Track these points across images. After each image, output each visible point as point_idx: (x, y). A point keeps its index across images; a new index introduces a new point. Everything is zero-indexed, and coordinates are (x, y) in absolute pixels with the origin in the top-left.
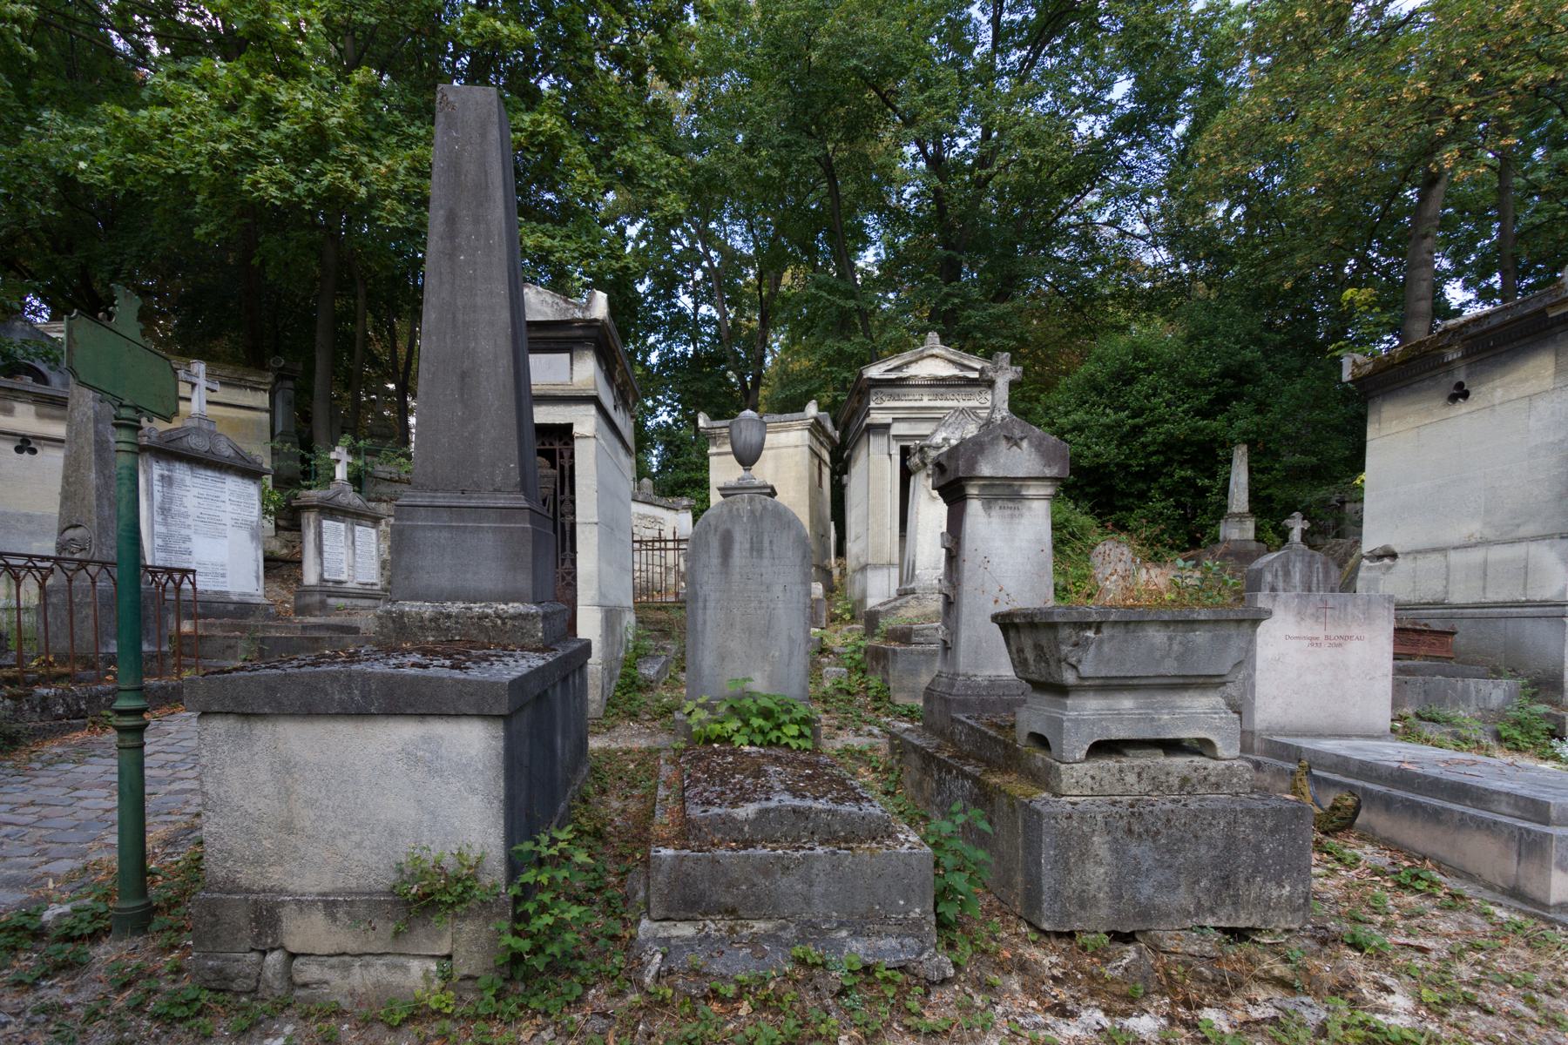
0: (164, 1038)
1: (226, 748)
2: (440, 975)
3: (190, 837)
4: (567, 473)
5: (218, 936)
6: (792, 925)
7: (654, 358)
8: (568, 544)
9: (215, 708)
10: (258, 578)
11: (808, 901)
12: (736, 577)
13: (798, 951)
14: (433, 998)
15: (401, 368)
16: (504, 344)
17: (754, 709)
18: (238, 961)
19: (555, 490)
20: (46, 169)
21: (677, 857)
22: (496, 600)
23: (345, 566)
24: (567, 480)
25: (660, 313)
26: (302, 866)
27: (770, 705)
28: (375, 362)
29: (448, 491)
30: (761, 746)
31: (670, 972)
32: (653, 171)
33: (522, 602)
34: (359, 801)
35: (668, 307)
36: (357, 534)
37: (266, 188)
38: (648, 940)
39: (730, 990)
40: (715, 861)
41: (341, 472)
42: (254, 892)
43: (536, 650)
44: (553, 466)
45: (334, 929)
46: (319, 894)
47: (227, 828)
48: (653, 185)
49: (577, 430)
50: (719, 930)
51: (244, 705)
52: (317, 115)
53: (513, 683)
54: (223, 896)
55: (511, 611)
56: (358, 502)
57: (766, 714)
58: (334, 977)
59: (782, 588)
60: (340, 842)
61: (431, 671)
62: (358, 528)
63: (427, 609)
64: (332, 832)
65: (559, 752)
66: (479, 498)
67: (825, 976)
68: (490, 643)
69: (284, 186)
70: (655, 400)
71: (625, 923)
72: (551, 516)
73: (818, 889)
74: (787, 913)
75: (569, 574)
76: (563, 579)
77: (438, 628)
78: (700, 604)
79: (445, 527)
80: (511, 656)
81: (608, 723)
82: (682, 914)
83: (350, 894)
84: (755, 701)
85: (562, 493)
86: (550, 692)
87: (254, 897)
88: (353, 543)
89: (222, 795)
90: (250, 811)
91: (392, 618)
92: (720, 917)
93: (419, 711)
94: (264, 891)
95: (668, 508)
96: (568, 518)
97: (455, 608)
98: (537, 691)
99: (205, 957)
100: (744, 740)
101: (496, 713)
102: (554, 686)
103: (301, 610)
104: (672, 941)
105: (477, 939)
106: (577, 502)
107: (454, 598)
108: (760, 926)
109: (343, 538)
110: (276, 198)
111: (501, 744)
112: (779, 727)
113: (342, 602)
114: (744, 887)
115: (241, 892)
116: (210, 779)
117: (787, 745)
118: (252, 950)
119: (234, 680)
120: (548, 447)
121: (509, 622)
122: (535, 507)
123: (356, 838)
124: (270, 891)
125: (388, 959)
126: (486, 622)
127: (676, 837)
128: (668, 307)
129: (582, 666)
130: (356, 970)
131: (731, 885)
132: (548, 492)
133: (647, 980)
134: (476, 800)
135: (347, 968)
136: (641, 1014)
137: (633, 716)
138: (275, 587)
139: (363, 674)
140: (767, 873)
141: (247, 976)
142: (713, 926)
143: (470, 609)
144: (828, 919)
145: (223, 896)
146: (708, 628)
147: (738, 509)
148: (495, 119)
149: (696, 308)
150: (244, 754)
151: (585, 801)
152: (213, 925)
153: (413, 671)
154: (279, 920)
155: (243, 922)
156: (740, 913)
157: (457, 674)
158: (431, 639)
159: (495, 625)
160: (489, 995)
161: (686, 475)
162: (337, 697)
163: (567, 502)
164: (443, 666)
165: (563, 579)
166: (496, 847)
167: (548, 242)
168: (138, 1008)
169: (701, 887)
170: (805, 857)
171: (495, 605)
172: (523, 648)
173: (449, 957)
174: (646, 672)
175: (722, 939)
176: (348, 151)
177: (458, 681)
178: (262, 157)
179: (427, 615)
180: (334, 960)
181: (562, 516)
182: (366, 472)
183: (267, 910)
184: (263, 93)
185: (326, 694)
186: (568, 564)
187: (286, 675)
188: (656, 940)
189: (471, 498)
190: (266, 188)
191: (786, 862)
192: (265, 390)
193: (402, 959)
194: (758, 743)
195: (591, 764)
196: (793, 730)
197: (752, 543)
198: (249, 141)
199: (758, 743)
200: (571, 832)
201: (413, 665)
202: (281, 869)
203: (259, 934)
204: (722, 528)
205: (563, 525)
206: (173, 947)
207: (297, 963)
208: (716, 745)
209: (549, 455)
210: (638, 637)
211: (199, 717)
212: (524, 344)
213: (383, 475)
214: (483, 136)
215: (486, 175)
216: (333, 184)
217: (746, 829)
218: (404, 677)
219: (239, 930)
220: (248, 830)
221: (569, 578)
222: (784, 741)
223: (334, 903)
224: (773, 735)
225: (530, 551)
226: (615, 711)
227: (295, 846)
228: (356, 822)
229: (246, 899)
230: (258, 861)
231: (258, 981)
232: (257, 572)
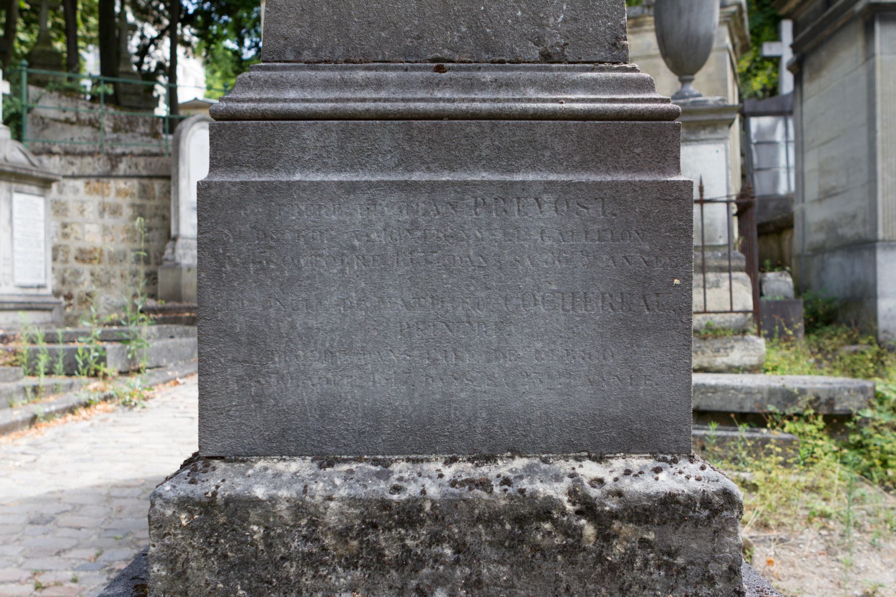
36: (16, 206)
62: (17, 197)
171: (564, 466)
179: (333, 514)
189: (471, 85)
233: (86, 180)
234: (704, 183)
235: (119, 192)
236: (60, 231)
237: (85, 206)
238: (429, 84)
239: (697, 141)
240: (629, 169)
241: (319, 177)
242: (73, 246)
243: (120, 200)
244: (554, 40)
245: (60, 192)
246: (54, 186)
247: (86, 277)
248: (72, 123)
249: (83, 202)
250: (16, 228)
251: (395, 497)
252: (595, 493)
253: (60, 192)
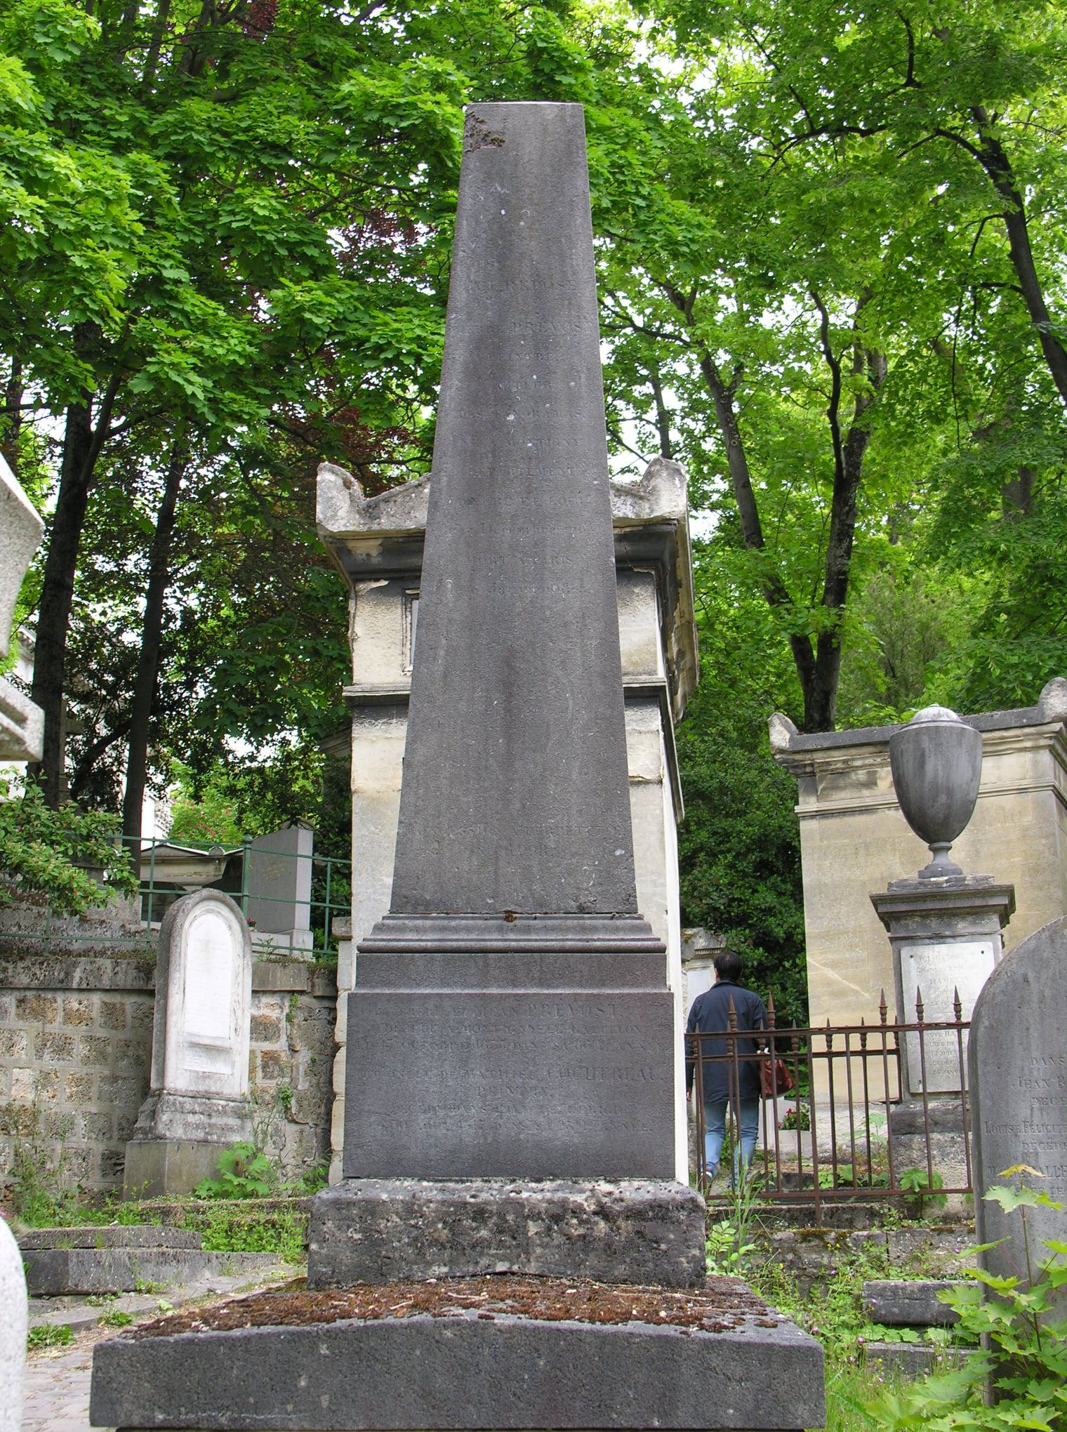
189: (528, 930)
234: (961, 999)
235: (68, 1017)
239: (953, 937)
241: (428, 991)
243: (69, 1030)
249: (12, 1032)
251: (457, 77)
252: (605, 1200)
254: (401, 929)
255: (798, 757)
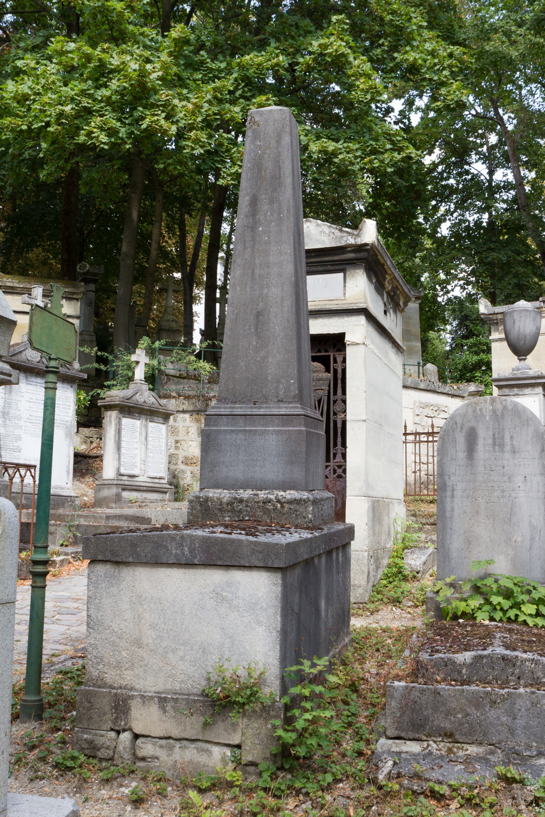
0: (61, 779)
1: (104, 585)
2: (233, 759)
3: (52, 668)
4: (339, 376)
5: (91, 718)
6: (499, 751)
7: (444, 230)
8: (339, 439)
9: (100, 557)
10: (68, 472)
11: (512, 731)
12: (481, 469)
13: (501, 769)
14: (228, 773)
15: (190, 256)
16: (289, 268)
17: (495, 587)
18: (102, 736)
19: (329, 391)
20: (461, 626)
21: (407, 687)
22: (278, 488)
23: (138, 461)
24: (339, 381)
25: (452, 181)
26: (145, 672)
27: (510, 585)
28: (164, 254)
29: (243, 403)
30: (501, 621)
31: (399, 775)
32: (435, 65)
33: (297, 490)
34: (184, 627)
35: (460, 174)
36: (150, 430)
37: (98, 136)
38: (384, 752)
39: (444, 790)
40: (437, 693)
41: (140, 373)
42: (114, 688)
43: (307, 528)
44: (328, 370)
45: (164, 718)
46: (155, 692)
47: (101, 641)
48: (436, 78)
49: (348, 338)
50: (440, 750)
51: (117, 556)
52: (143, 74)
53: (288, 544)
54: (96, 689)
55: (288, 497)
56: (152, 400)
57: (508, 594)
58: (161, 753)
59: (522, 478)
60: (170, 655)
61: (233, 536)
62: (151, 424)
63: (225, 495)
64: (165, 648)
65: (323, 613)
66: (267, 408)
67: (522, 789)
68: (272, 522)
69: (112, 132)
70: (447, 274)
71: (368, 742)
72: (324, 419)
73: (520, 722)
74: (495, 740)
75: (340, 467)
76: (335, 471)
77: (233, 511)
78: (449, 493)
79: (240, 431)
80: (287, 531)
81: (371, 606)
82: (411, 735)
83: (175, 694)
84: (496, 581)
85: (335, 393)
86: (316, 561)
87: (115, 691)
88: (146, 438)
89: (99, 618)
90: (116, 630)
91: (199, 502)
92: (440, 739)
93: (226, 563)
94: (121, 688)
95: (453, 396)
96: (340, 416)
97: (246, 494)
98: (306, 556)
99: (82, 732)
100: (486, 616)
101: (276, 566)
102: (319, 556)
103: (98, 503)
104: (403, 755)
105: (259, 734)
106: (348, 402)
107: (245, 487)
108: (473, 750)
109: (137, 434)
110: (104, 143)
111: (280, 589)
112: (517, 605)
113: (133, 495)
114: (460, 716)
115: (107, 688)
116: (93, 607)
117: (525, 623)
118: (112, 730)
119: (112, 539)
120: (323, 354)
121: (287, 506)
122: (310, 413)
123: (181, 653)
124: (125, 688)
125: (200, 744)
126: (270, 506)
127: (408, 676)
128: (460, 174)
129: (346, 546)
130: (177, 750)
131: (448, 713)
132: (323, 394)
133: (381, 777)
134: (261, 630)
135: (171, 748)
136: (375, 801)
137: (396, 602)
138: (77, 483)
139: (190, 536)
140: (478, 706)
141: (108, 748)
142: (434, 746)
143: (257, 495)
144: (529, 747)
145: (96, 689)
146: (456, 515)
147: (481, 410)
148: (287, 129)
149: (491, 173)
150: (114, 590)
151: (344, 664)
152: (89, 709)
153: (222, 535)
154: (129, 709)
155: (107, 709)
156: (457, 737)
157: (251, 538)
158: (227, 519)
159: (275, 508)
160: (266, 776)
161: (475, 358)
162: (174, 552)
163: (339, 402)
164: (240, 534)
165: (335, 471)
166: (274, 666)
167: (331, 146)
168: (43, 759)
169: (425, 713)
170: (509, 694)
171: (276, 492)
172: (296, 527)
173: (239, 747)
174: (412, 562)
175: (442, 757)
176: (164, 98)
177: (251, 542)
178: (97, 111)
179: (225, 500)
180: (163, 742)
181: (335, 414)
182: (160, 370)
183: (123, 702)
184: (100, 60)
185: (168, 550)
186: (339, 458)
187: (144, 536)
188: (390, 753)
190: (98, 136)
191: (493, 697)
192: (77, 299)
193: (208, 746)
194: (498, 619)
195: (352, 636)
196: (530, 609)
197: (494, 439)
198: (87, 100)
199: (498, 619)
200: (326, 661)
201: (221, 532)
202: (132, 673)
203: (117, 718)
204: (468, 425)
205: (335, 422)
206: (59, 730)
207: (139, 741)
208: (461, 621)
209: (325, 361)
210: (408, 529)
211: (89, 563)
212: (304, 268)
213: (172, 372)
214: (279, 142)
215: (280, 169)
216: (150, 126)
217: (464, 671)
218: (216, 539)
219: (105, 714)
220: (113, 644)
221: (340, 471)
222: (521, 619)
223: (165, 699)
224: (512, 614)
225: (304, 449)
226: (380, 596)
227: (142, 657)
228: (181, 642)
229: (110, 692)
230: (118, 666)
231: (114, 752)
232: (68, 468)
233: (191, 414)
236: (174, 445)
237: (189, 429)
238: (251, 408)
240: (293, 427)
242: (181, 454)
244: (281, 396)
245: (175, 421)
246: (172, 417)
247: (188, 474)
248: (184, 378)
250: (149, 442)
253: (175, 421)
254: (219, 408)
255: (490, 316)
